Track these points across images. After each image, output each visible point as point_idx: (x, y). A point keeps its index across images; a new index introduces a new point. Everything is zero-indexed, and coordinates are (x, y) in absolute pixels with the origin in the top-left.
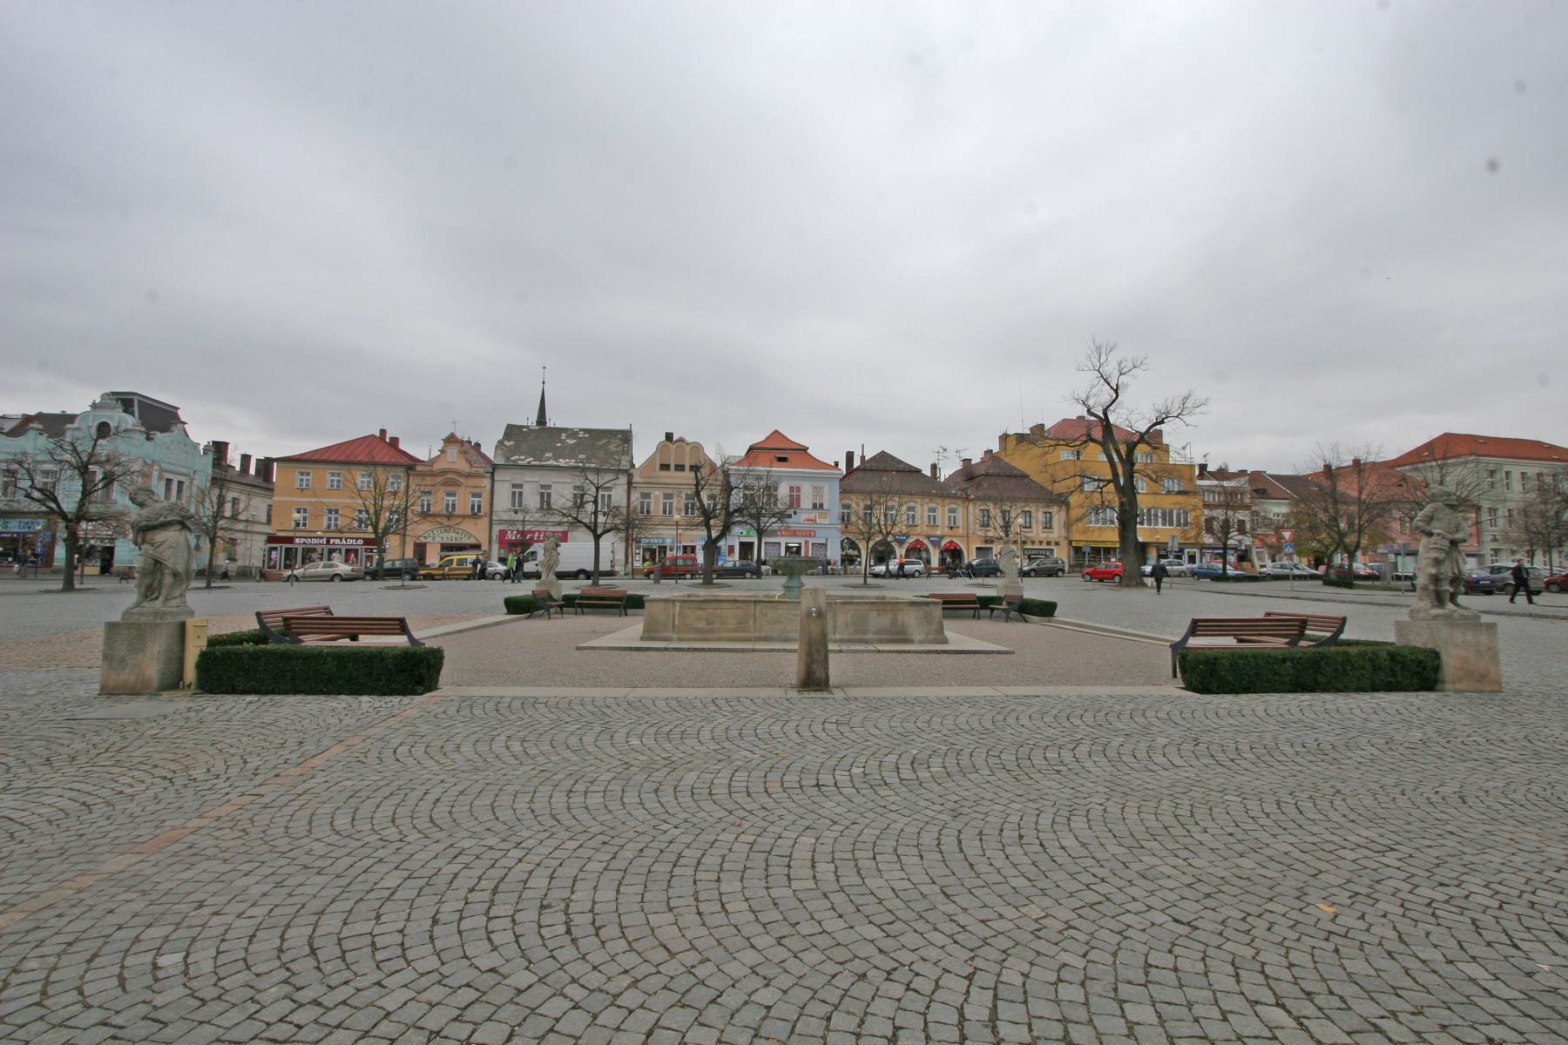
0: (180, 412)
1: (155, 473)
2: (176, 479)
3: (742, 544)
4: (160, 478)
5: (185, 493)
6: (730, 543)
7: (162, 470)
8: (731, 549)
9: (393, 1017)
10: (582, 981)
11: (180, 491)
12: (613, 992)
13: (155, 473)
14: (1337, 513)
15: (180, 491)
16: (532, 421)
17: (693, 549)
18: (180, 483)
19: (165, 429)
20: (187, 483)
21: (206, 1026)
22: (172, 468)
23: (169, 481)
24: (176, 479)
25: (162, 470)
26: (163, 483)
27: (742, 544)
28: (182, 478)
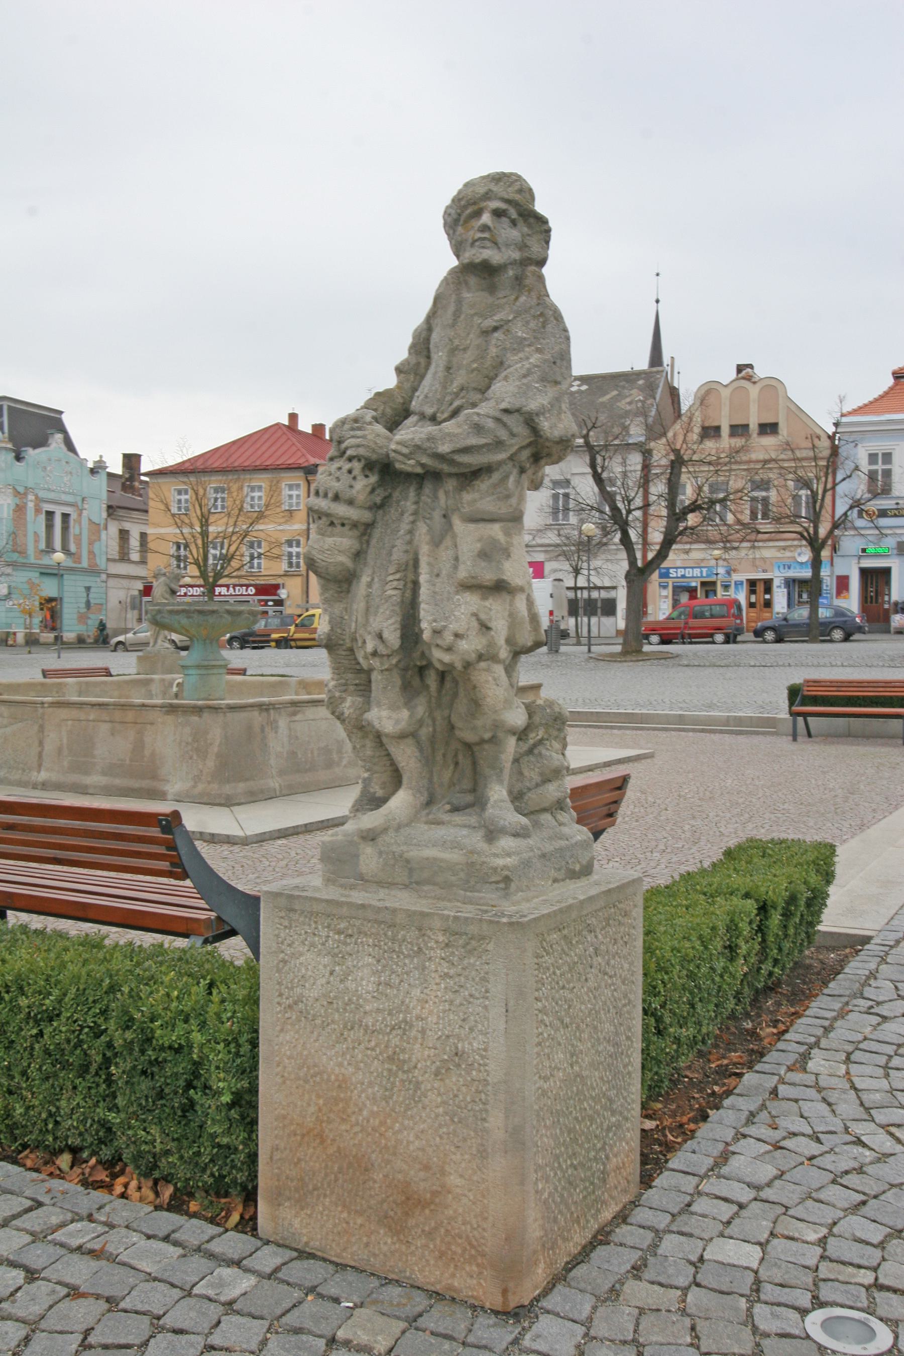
0: (65, 418)
1: (31, 505)
2: (59, 511)
3: (865, 573)
4: (38, 511)
5: (74, 530)
6: (840, 571)
7: (39, 500)
8: (843, 584)
9: (786, 1177)
10: (176, 1293)
11: (65, 528)
12: (137, 1341)
13: (31, 505)
14: (104, 1161)
15: (65, 528)
16: (642, 363)
17: (768, 585)
18: (65, 516)
19: (41, 442)
20: (74, 516)
21: (824, 1106)
22: (51, 496)
23: (50, 514)
24: (59, 511)
25: (39, 500)
26: (42, 517)
27: (865, 573)
28: (67, 510)
